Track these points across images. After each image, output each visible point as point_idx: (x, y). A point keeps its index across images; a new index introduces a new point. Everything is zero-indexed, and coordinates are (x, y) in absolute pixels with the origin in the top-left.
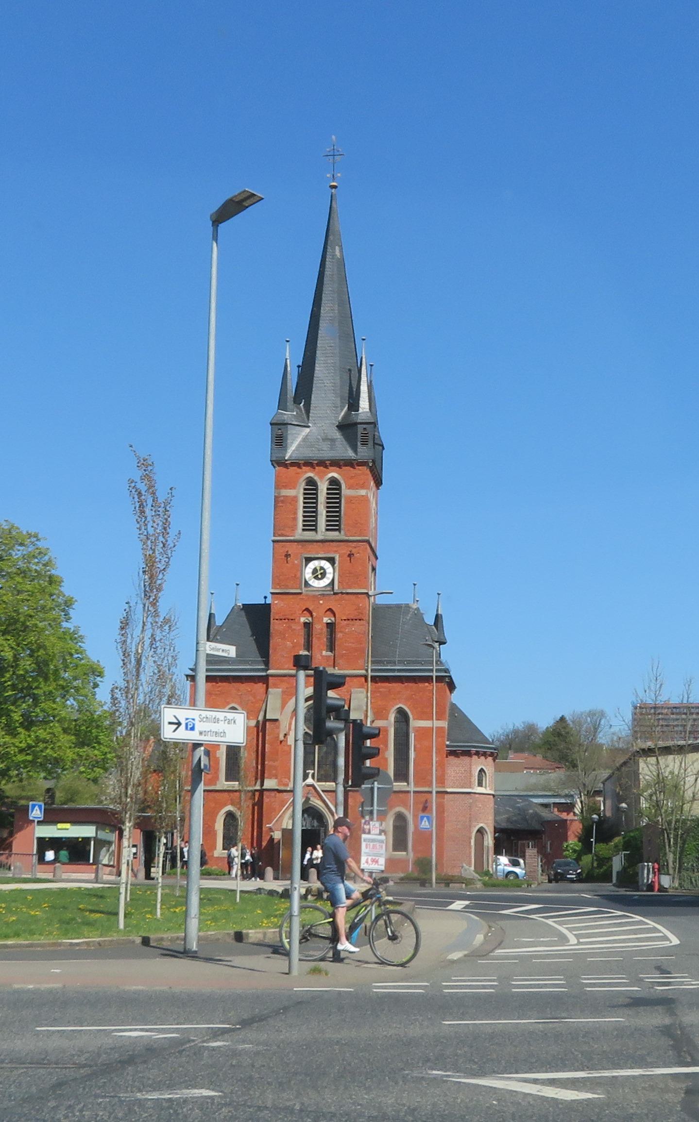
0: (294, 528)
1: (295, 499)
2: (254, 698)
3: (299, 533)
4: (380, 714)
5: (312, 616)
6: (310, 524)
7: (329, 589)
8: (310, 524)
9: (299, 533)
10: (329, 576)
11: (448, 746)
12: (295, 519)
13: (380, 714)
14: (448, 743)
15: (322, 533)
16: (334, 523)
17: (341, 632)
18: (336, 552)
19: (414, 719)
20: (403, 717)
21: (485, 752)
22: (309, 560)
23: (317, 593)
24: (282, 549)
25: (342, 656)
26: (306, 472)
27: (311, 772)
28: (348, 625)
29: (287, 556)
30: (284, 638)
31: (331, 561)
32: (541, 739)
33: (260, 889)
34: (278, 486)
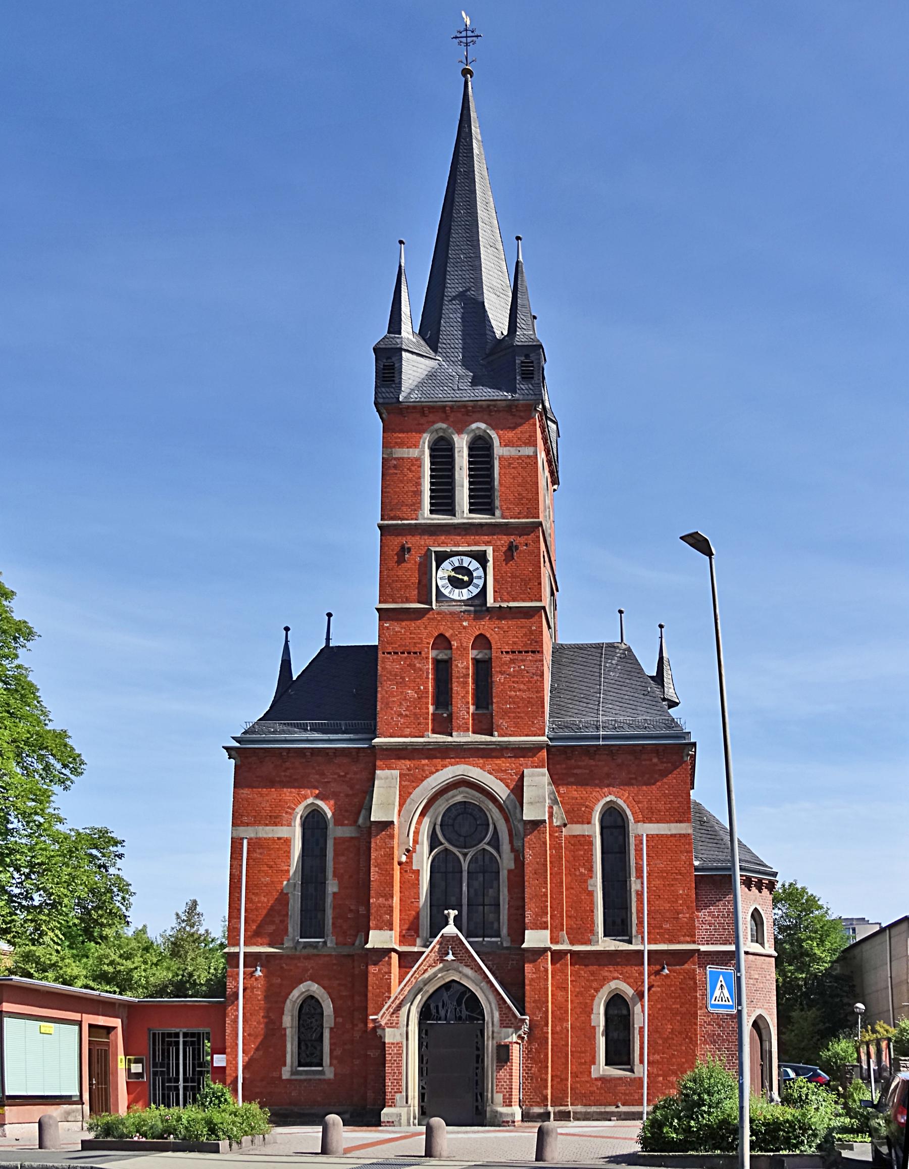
0: (418, 505)
1: (418, 462)
2: (352, 788)
3: (426, 515)
4: (578, 815)
5: (450, 647)
6: (443, 500)
7: (477, 602)
8: (443, 500)
9: (426, 515)
10: (456, 594)
11: (697, 869)
12: (418, 493)
13: (578, 815)
14: (696, 863)
15: (464, 513)
16: (482, 500)
17: (501, 673)
18: (487, 543)
19: (637, 822)
20: (614, 825)
21: (760, 880)
22: (441, 558)
23: (458, 609)
24: (396, 542)
25: (506, 713)
26: (434, 423)
27: (453, 913)
28: (512, 661)
29: (404, 553)
30: (402, 684)
31: (481, 558)
32: (377, 1027)
33: (375, 404)
34: (385, 445)
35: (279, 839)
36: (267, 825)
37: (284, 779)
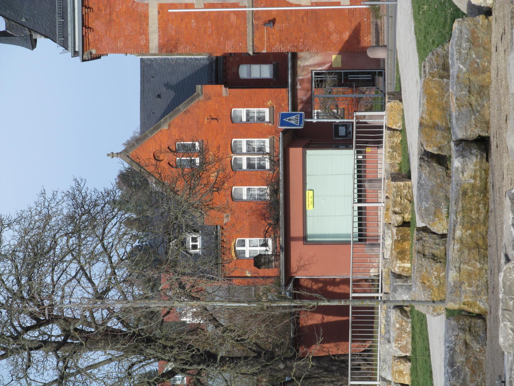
35: (159, 13)
36: (147, 24)
37: (108, 11)
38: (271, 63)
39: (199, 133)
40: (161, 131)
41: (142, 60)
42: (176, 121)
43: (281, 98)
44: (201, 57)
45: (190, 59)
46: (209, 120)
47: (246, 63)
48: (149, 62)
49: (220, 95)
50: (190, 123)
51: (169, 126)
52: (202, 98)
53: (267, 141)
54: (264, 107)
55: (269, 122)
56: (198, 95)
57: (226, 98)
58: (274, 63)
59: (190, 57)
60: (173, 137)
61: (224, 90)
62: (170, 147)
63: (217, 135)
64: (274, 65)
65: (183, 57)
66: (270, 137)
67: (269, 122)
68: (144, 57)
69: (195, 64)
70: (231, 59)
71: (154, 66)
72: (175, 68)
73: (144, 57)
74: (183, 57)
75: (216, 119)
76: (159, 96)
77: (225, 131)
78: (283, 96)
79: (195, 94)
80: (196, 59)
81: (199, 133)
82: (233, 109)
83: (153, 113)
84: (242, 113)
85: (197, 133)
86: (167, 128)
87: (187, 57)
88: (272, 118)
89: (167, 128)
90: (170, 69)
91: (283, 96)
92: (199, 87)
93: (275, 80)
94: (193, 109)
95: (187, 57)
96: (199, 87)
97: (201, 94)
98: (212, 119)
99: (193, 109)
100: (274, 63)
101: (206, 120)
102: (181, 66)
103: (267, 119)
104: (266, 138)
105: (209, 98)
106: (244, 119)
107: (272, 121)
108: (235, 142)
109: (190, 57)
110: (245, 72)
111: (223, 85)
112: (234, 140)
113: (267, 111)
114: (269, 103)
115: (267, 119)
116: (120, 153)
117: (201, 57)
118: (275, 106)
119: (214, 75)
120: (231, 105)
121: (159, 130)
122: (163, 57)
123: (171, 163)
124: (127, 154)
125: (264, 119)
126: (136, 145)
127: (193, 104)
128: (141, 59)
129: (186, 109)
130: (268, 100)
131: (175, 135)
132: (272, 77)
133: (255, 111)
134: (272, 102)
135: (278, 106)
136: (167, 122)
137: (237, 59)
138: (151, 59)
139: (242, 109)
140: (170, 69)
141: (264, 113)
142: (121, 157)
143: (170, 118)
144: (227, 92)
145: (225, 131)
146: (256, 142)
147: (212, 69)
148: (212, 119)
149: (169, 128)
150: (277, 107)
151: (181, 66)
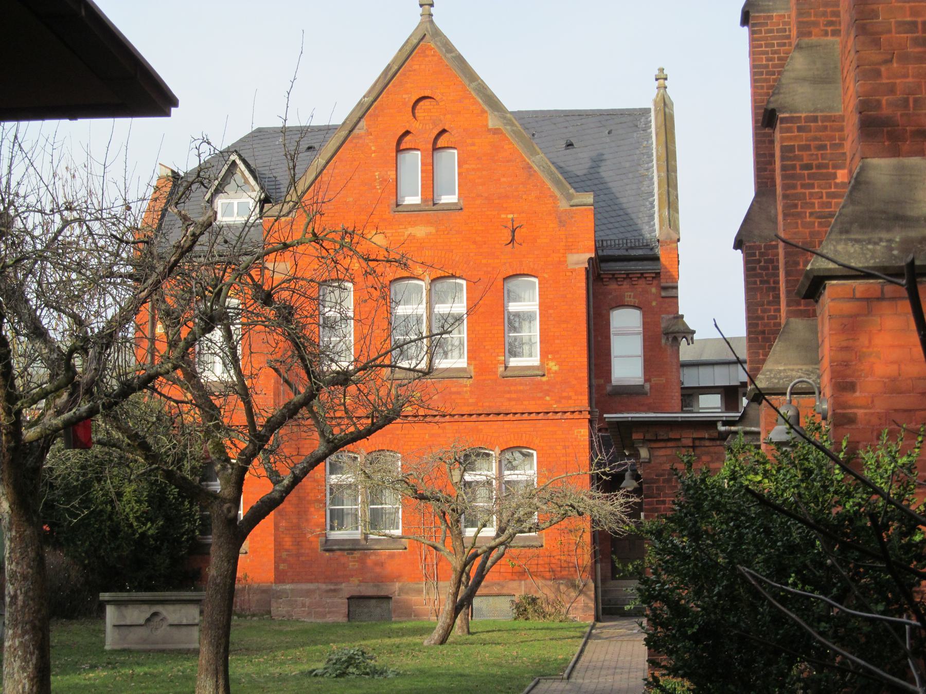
38: (646, 381)
39: (478, 202)
40: (483, 111)
41: (646, 111)
42: (506, 147)
43: (565, 394)
44: (657, 227)
45: (652, 203)
46: (510, 225)
47: (645, 324)
48: (642, 125)
49: (569, 249)
50: (503, 180)
51: (496, 131)
52: (563, 205)
53: (462, 363)
54: (544, 354)
55: (506, 367)
56: (569, 197)
57: (562, 262)
58: (647, 386)
59: (656, 203)
60: (469, 141)
61: (580, 259)
62: (446, 134)
63: (475, 242)
64: (643, 386)
65: (656, 190)
66: (472, 368)
67: (506, 367)
68: (653, 114)
69: (640, 215)
70: (654, 290)
71: (635, 135)
72: (630, 175)
73: (653, 114)
74: (656, 190)
75: (513, 240)
76: (570, 145)
77: (484, 261)
78: (569, 398)
79: (572, 191)
80: (651, 217)
81: (478, 202)
82: (536, 280)
83: (533, 135)
84: (526, 301)
85: (479, 196)
86: (490, 126)
87: (656, 197)
88: (516, 373)
89: (490, 126)
90: (628, 164)
91: (569, 398)
92: (589, 198)
93: (609, 388)
94: (536, 185)
95: (656, 197)
96: (589, 198)
97: (572, 203)
98: (514, 231)
99: (536, 185)
100: (647, 386)
101: (510, 216)
102: (635, 187)
103: (514, 362)
104: (469, 358)
105: (562, 223)
106: (513, 307)
107: (508, 373)
108: (532, 455)
109: (656, 203)
110: (626, 323)
111: (593, 255)
112: (535, 453)
113: (535, 361)
114: (553, 366)
115: (514, 362)
116: (432, 22)
117: (657, 227)
118: (544, 379)
119: (617, 253)
120: (546, 276)
121: (486, 108)
122: (654, 152)
123: (408, 138)
124: (428, 36)
125: (515, 355)
126: (449, 56)
127: (549, 184)
128: (650, 109)
129: (536, 168)
130: (559, 363)
131: (473, 144)
132: (614, 382)
133: (532, 332)
134: (556, 372)
135: (545, 387)
136: (505, 124)
137: (654, 304)
138: (650, 127)
139: (537, 302)
140: (628, 164)
141: (530, 355)
142: (421, 23)
143: (514, 132)
144: (577, 264)
145: (484, 261)
146: (460, 335)
147: (632, 248)
148: (514, 231)
149: (489, 130)
150: (544, 383)
151: (635, 187)
